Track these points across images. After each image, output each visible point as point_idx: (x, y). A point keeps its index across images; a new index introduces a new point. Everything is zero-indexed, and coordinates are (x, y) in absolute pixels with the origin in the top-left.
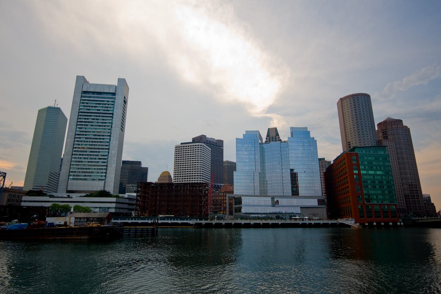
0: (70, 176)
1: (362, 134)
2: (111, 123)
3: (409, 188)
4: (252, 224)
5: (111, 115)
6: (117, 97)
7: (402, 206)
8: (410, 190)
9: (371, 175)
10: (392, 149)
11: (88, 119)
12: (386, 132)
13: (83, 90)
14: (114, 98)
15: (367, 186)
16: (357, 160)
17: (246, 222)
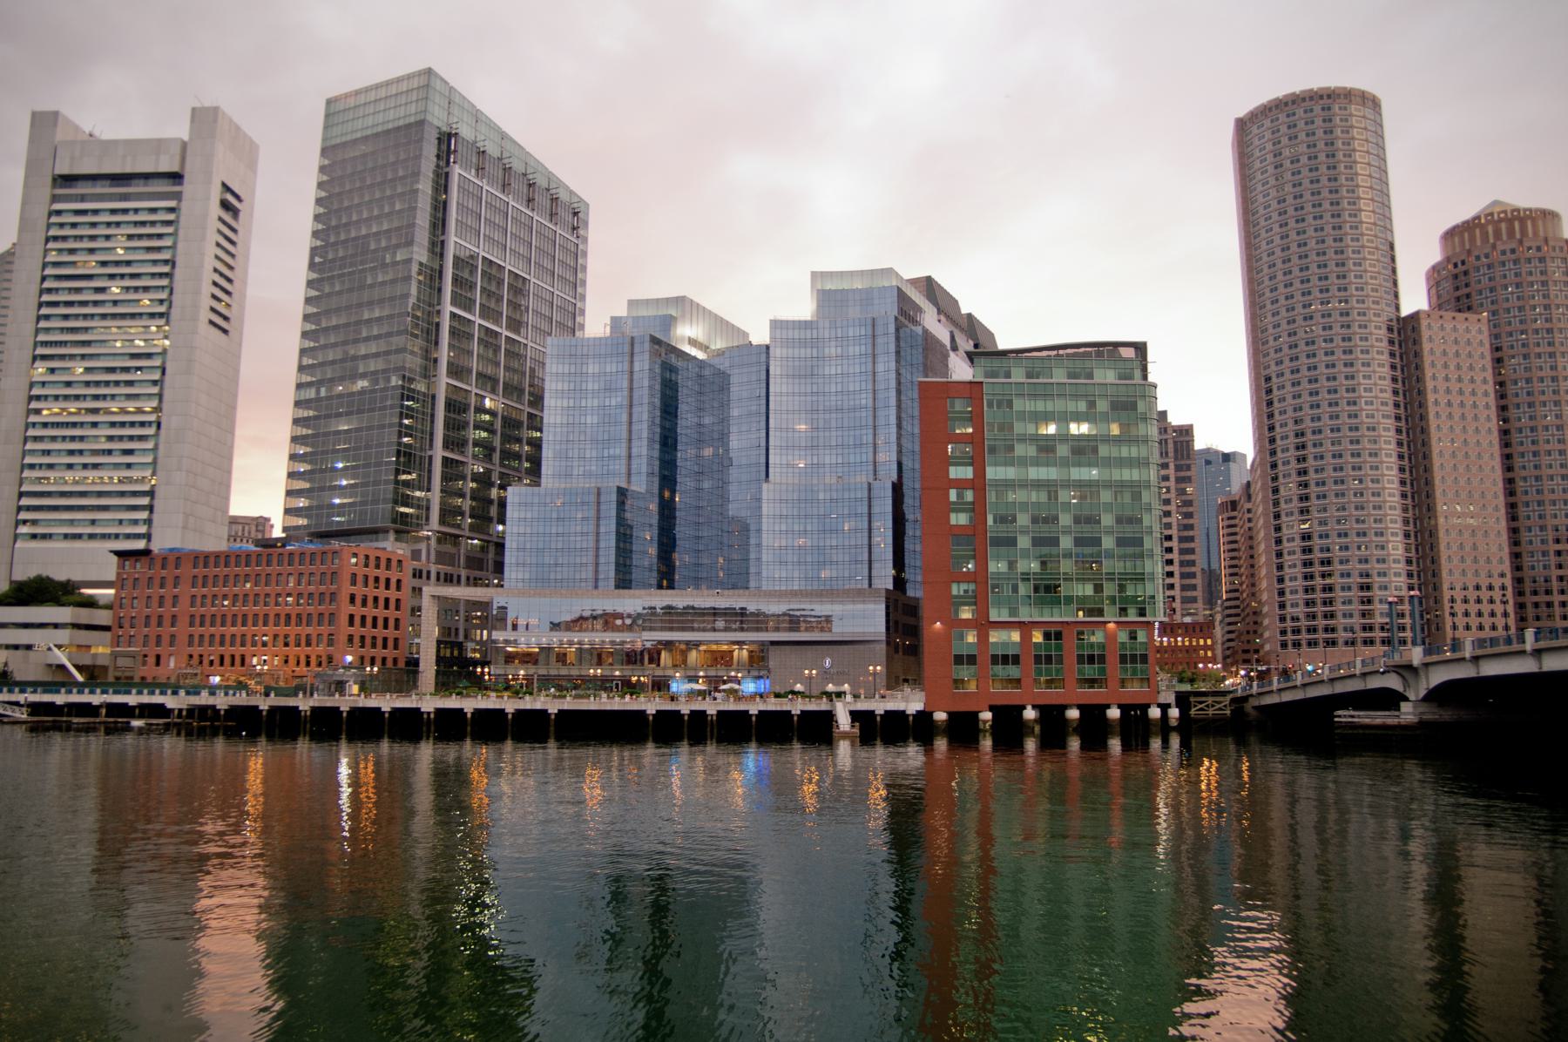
2: (166, 304)
4: (429, 713)
5: (166, 269)
6: (187, 188)
7: (1494, 628)
9: (1038, 485)
10: (1470, 355)
11: (78, 290)
12: (1466, 273)
13: (57, 172)
14: (178, 196)
15: (1012, 542)
16: (976, 419)
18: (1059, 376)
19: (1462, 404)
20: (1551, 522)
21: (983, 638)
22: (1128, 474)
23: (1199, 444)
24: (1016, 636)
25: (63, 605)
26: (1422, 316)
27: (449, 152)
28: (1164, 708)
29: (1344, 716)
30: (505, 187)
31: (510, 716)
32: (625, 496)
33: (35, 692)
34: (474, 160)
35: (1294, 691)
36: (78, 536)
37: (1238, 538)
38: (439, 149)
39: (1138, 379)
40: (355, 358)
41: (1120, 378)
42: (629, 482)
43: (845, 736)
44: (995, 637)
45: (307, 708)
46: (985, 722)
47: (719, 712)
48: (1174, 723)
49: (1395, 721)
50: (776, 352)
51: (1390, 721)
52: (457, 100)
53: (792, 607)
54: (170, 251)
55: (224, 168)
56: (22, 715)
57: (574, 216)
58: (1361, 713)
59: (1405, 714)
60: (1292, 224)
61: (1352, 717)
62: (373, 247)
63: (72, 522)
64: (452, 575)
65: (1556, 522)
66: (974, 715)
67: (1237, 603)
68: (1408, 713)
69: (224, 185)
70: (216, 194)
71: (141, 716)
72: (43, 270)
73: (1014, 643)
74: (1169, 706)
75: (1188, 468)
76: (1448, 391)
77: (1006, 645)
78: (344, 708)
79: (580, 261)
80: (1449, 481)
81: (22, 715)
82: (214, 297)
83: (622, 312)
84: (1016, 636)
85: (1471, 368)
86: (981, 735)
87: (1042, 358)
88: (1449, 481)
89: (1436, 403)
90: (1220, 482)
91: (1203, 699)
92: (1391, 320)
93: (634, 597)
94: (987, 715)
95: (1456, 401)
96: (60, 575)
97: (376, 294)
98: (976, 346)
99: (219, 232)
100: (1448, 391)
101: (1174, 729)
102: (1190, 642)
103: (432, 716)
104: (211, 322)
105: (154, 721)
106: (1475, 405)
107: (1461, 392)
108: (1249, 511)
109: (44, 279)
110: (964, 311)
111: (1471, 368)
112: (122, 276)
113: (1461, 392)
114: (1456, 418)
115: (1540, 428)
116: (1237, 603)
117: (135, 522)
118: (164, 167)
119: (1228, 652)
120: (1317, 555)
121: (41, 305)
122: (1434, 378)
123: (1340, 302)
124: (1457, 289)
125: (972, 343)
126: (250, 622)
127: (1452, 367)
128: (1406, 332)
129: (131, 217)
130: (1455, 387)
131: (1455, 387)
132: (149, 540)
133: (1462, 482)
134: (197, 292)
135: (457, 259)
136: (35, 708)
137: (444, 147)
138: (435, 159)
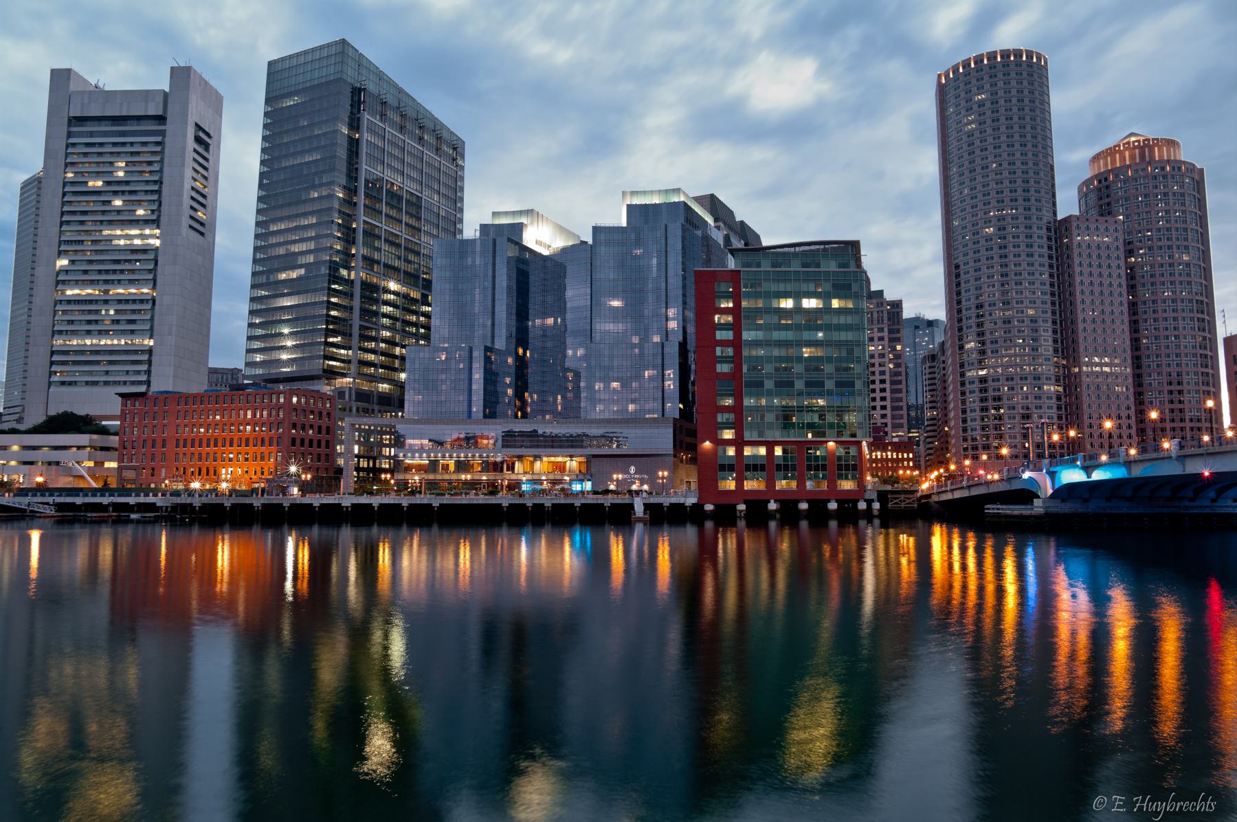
0: (52, 377)
1: (1011, 200)
3: (1165, 385)
4: (347, 507)
5: (156, 188)
6: (169, 127)
8: (1171, 392)
14: (162, 133)
17: (325, 501)
18: (795, 266)
19: (1101, 284)
20: (1165, 369)
21: (739, 452)
22: (844, 336)
23: (907, 313)
24: (762, 451)
25: (84, 433)
26: (1073, 219)
27: (359, 103)
28: (869, 502)
29: (991, 509)
30: (402, 129)
31: (405, 509)
32: (251, 336)
33: (60, 496)
34: (378, 108)
35: (962, 491)
36: (95, 383)
37: (936, 381)
38: (352, 100)
39: (852, 268)
40: (295, 254)
41: (840, 267)
42: (493, 343)
43: (640, 520)
44: (748, 451)
45: (259, 505)
46: (741, 511)
47: (553, 505)
48: (876, 513)
49: (1028, 512)
50: (602, 250)
51: (1025, 513)
52: (365, 64)
53: (606, 431)
54: (159, 175)
55: (196, 112)
56: (51, 511)
57: (457, 149)
58: (1004, 507)
59: (1037, 507)
60: (978, 152)
61: (998, 509)
62: (305, 172)
63: (90, 373)
64: (368, 409)
65: (1169, 370)
66: (733, 507)
67: (935, 428)
68: (1038, 506)
69: (196, 124)
70: (191, 132)
71: (138, 512)
72: (64, 188)
73: (762, 456)
74: (872, 501)
75: (898, 331)
76: (1091, 274)
77: (755, 457)
78: (286, 504)
79: (459, 184)
80: (1090, 340)
81: (51, 511)
82: (192, 208)
83: (488, 220)
84: (762, 451)
85: (1109, 257)
86: (738, 520)
87: (784, 253)
88: (1090, 340)
89: (1082, 283)
90: (926, 341)
91: (898, 496)
92: (1050, 223)
93: (496, 424)
94: (742, 507)
95: (1097, 281)
96: (81, 411)
97: (308, 208)
98: (746, 244)
99: (195, 160)
100: (1091, 274)
101: (876, 516)
102: (897, 455)
103: (350, 509)
104: (191, 227)
105: (148, 515)
106: (1111, 285)
107: (1100, 275)
108: (944, 362)
109: (64, 194)
110: (738, 219)
111: (1109, 257)
112: (123, 192)
113: (1100, 275)
114: (1097, 294)
115: (1159, 301)
116: (935, 428)
117: (138, 372)
118: (152, 111)
119: (928, 463)
120: (991, 393)
121: (63, 214)
122: (1080, 264)
123: (1012, 209)
124: (1101, 199)
125: (743, 242)
126: (220, 444)
127: (1094, 257)
128: (1060, 229)
129: (128, 149)
130: (1096, 271)
131: (1096, 271)
132: (149, 386)
133: (1100, 341)
134: (180, 204)
135: (367, 181)
136: (60, 507)
137: (356, 99)
138: (349, 108)
